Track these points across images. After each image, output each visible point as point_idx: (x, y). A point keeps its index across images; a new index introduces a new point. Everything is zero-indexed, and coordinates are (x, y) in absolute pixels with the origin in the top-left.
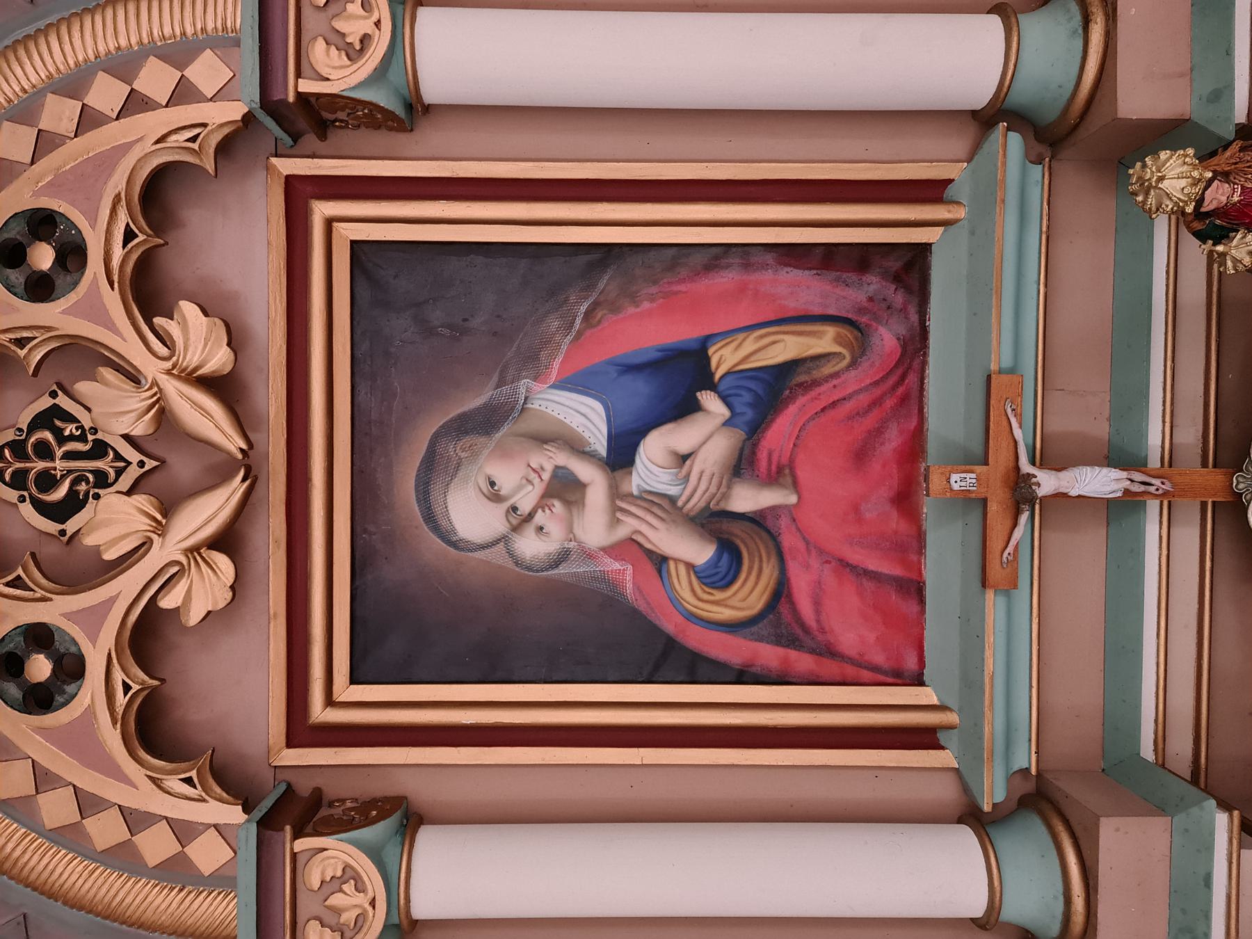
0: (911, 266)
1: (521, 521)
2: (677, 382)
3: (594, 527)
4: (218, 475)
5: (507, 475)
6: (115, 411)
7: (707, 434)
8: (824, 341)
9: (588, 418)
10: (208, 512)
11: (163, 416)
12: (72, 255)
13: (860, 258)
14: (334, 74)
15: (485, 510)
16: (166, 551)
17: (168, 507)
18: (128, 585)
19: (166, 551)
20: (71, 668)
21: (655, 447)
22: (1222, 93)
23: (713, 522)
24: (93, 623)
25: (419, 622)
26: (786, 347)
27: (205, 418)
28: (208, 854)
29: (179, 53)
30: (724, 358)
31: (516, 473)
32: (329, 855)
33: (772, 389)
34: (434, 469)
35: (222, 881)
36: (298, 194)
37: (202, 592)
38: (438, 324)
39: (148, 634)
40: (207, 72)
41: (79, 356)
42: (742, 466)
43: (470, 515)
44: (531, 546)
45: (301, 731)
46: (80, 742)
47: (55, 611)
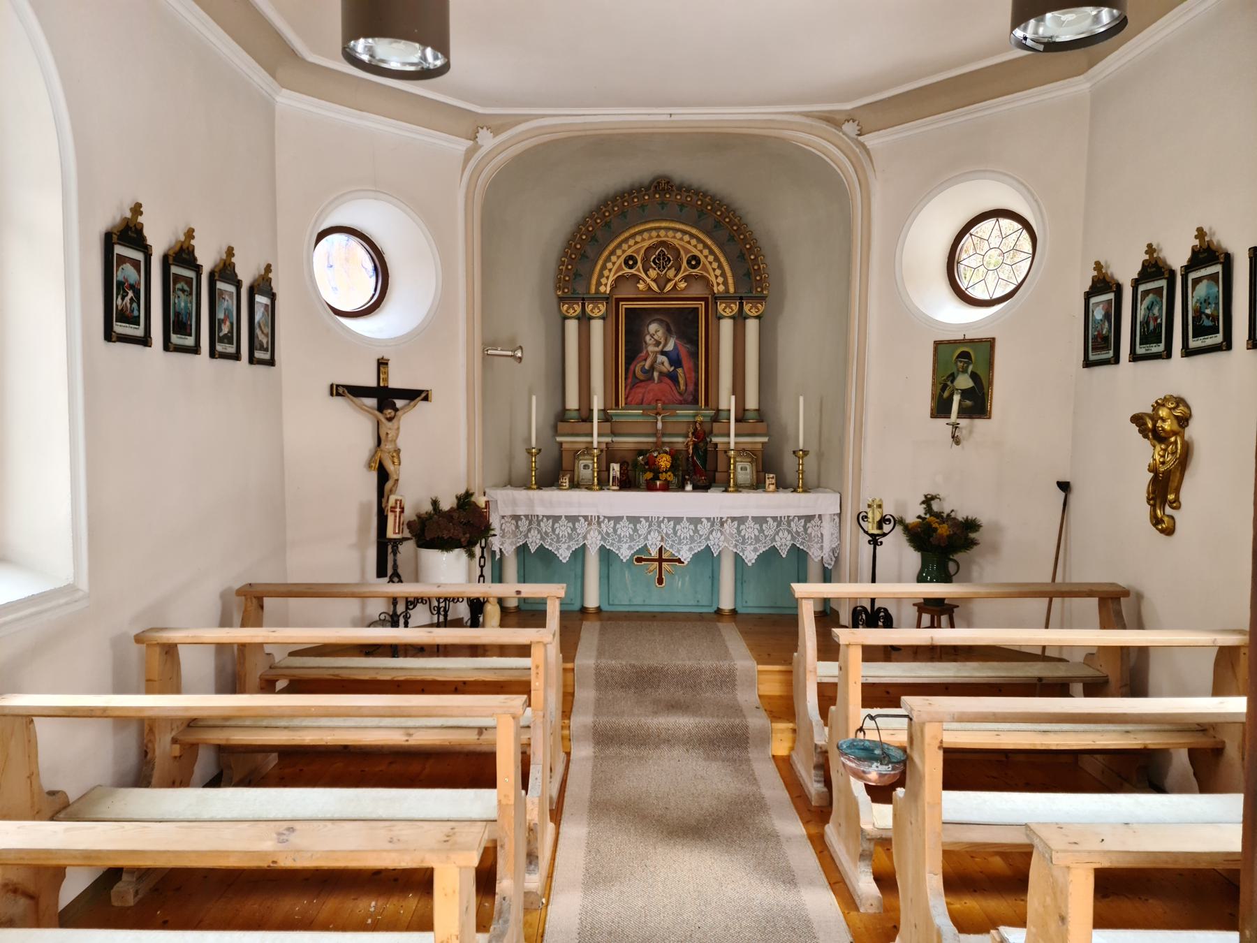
0: (695, 401)
1: (652, 336)
2: (675, 361)
3: (651, 349)
4: (662, 288)
5: (660, 334)
6: (671, 273)
7: (667, 367)
8: (682, 387)
9: (670, 347)
10: (654, 286)
11: (669, 280)
12: (694, 267)
13: (696, 390)
14: (721, 307)
15: (655, 329)
16: (648, 280)
17: (654, 281)
18: (643, 275)
19: (648, 280)
20: (631, 267)
21: (664, 359)
22: (716, 436)
23: (652, 368)
24: (638, 270)
25: (636, 320)
26: (682, 381)
27: (669, 286)
28: (602, 289)
29: (725, 283)
30: (680, 371)
31: (660, 335)
32: (603, 308)
33: (673, 378)
34: (661, 322)
35: (597, 289)
36: (705, 299)
37: (641, 286)
38: (688, 325)
39: (637, 279)
40: (722, 288)
41: (678, 270)
42: (661, 373)
43: (653, 327)
44: (648, 338)
45: (618, 300)
46: (620, 268)
47: (639, 264)
